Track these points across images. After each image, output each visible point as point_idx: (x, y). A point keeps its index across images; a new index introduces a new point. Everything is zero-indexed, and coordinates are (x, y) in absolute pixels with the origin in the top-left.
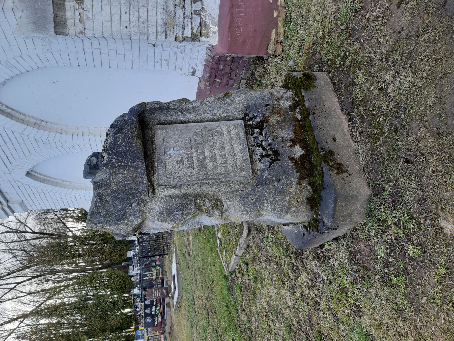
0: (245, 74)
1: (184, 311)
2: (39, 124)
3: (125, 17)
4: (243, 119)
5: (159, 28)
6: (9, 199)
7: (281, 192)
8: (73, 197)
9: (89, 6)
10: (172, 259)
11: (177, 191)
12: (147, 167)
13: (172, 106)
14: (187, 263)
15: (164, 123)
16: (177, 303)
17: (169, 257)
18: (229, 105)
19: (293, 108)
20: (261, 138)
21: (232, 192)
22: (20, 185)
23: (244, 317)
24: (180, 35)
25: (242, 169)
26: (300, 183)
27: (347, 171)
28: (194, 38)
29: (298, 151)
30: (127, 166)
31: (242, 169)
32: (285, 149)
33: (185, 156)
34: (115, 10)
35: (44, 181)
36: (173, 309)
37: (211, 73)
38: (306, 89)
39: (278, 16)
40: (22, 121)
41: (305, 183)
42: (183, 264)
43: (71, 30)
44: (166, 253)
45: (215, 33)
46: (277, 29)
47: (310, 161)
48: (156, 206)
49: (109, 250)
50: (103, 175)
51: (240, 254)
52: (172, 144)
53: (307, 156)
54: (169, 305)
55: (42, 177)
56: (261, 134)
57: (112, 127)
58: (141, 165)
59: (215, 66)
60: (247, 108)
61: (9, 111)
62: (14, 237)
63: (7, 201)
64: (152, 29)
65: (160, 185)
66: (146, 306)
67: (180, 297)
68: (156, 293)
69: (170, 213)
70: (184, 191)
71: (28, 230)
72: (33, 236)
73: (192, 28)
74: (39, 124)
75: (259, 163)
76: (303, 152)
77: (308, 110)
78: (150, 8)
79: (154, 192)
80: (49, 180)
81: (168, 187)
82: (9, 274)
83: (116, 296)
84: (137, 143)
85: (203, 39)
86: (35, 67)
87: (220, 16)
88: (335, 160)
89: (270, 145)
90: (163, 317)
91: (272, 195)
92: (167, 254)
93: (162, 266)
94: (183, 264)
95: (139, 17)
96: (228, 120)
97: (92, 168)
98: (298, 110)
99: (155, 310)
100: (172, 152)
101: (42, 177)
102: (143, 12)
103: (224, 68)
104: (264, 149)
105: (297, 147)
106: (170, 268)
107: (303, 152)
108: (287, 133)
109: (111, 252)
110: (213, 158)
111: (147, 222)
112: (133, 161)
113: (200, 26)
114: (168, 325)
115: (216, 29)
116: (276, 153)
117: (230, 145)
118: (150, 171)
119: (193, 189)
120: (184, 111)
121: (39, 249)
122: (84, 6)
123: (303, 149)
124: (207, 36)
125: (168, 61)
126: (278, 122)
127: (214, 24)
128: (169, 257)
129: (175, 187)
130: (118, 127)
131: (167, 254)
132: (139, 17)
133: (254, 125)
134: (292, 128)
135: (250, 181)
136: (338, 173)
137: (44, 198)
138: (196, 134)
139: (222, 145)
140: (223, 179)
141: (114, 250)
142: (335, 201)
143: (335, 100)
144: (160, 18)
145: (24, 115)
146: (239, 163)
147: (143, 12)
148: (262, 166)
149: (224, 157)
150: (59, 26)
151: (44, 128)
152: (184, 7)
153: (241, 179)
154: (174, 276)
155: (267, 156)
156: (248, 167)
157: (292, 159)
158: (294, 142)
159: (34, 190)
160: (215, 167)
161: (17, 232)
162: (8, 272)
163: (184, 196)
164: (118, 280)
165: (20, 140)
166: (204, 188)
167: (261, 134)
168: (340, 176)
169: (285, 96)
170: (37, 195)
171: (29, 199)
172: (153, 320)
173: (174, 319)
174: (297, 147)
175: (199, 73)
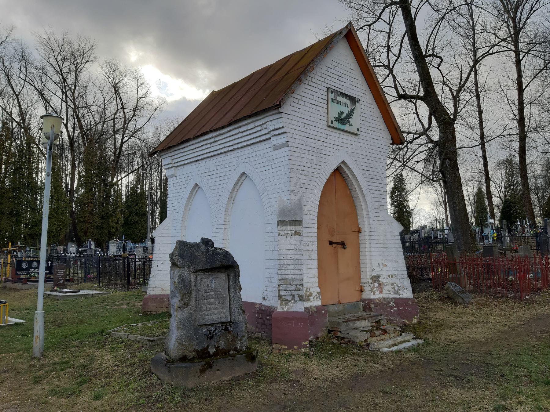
0: (265, 336)
2: (231, 199)
3: (289, 257)
4: (230, 322)
5: (284, 276)
6: (178, 168)
7: (190, 340)
8: (177, 211)
9: (293, 238)
10: (94, 290)
11: (193, 284)
12: (206, 269)
13: (237, 282)
14: (96, 304)
15: (228, 278)
16: (49, 295)
17: (96, 287)
18: (238, 313)
19: (236, 349)
20: (220, 330)
21: (191, 313)
22: (189, 178)
23: (75, 343)
24: (281, 288)
25: (203, 319)
26: (195, 351)
27: (201, 375)
28: (280, 297)
29: (212, 350)
30: (207, 259)
31: (203, 319)
32: (213, 343)
33: (211, 288)
34: (292, 252)
35: (191, 193)
37: (264, 311)
38: (246, 357)
39: (295, 349)
40: (233, 190)
41: (194, 353)
42: (94, 300)
43: (280, 228)
44: (101, 284)
45: (283, 309)
46: (287, 349)
47: (207, 357)
49: (94, 221)
50: (203, 248)
51: (129, 338)
52: (217, 282)
53: (210, 356)
55: (194, 193)
56: (222, 330)
57: (227, 252)
58: (207, 266)
59: (268, 313)
60: (237, 323)
61: (240, 183)
62: (119, 126)
63: (176, 167)
64: (283, 272)
65: (197, 275)
67: (57, 298)
69: (182, 280)
70: (193, 287)
71: (125, 139)
72: (119, 143)
73: (285, 295)
74: (231, 199)
75: (206, 329)
76: (211, 353)
77: (234, 356)
78: (294, 271)
79: (194, 272)
80: (191, 196)
81: (196, 280)
82: (77, 117)
84: (218, 264)
85: (279, 302)
86: (264, 204)
87: (293, 312)
88: (206, 369)
89: (216, 334)
91: (189, 335)
92: (99, 284)
93: (86, 280)
94: (94, 300)
95: (289, 265)
96: (230, 313)
97: (207, 242)
98: (235, 352)
100: (213, 282)
101: (194, 193)
102: (292, 267)
103: (268, 320)
104: (214, 331)
105: (214, 350)
106: (84, 288)
107: (211, 353)
108: (222, 345)
109: (91, 223)
110: (210, 303)
111: (178, 269)
112: (209, 262)
113: (286, 300)
114: (19, 286)
115: (286, 310)
116: (211, 338)
117: (217, 313)
118: (204, 271)
119: (194, 292)
120: (235, 288)
121: (102, 149)
122: (293, 236)
123: (213, 353)
124: (281, 304)
125: (270, 282)
126: (228, 339)
127: (288, 308)
128: (96, 287)
129: (195, 283)
130: (227, 255)
131: (99, 284)
132: (289, 265)
133: (227, 326)
134: (225, 347)
135: (197, 324)
136: (200, 369)
137: (177, 191)
138: (222, 295)
139: (216, 309)
140: (198, 308)
141: (94, 226)
142: (186, 367)
143: (240, 374)
144: (289, 277)
145: (237, 191)
146: (206, 317)
147: (292, 267)
148: (204, 331)
149: (210, 309)
150: (281, 223)
151: (229, 202)
152: (296, 290)
153: (198, 319)
154: (79, 291)
155: (210, 333)
156: (204, 322)
157: (208, 347)
158: (217, 348)
159: (185, 186)
160: (205, 304)
161: (124, 129)
162: (80, 116)
163: (190, 288)
164: (56, 230)
165: (221, 186)
166: (194, 298)
167: (222, 330)
168: (199, 371)
169: (243, 345)
170: (180, 187)
171: (177, 181)
172: (24, 270)
173: (28, 292)
174: (214, 350)
175: (264, 303)
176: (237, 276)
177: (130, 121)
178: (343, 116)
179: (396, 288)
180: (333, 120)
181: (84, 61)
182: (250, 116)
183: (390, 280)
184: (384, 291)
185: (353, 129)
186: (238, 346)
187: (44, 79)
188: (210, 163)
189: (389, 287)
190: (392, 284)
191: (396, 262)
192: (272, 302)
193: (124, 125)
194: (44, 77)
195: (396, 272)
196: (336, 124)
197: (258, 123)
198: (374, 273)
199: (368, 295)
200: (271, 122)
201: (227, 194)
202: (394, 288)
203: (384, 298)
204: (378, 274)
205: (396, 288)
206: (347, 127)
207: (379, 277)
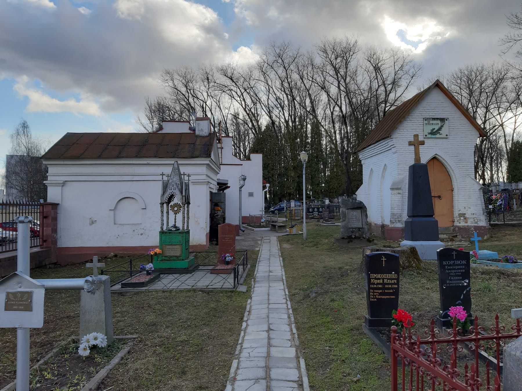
1: (316, 227)
19: (363, 237)
29: (353, 237)
32: (354, 234)
36: (317, 223)
48: (344, 210)
52: (357, 213)
54: (319, 221)
66: (318, 209)
68: (326, 214)
83: (323, 185)
90: (312, 218)
99: (316, 214)
108: (357, 235)
176: (366, 211)
177: (390, 93)
178: (434, 131)
179: (476, 221)
180: (427, 134)
181: (351, 53)
182: (383, 139)
183: (472, 216)
184: (469, 222)
185: (444, 136)
186: (364, 236)
187: (325, 74)
188: (374, 159)
189: (472, 220)
190: (474, 218)
191: (476, 206)
192: (387, 222)
193: (386, 97)
194: (325, 73)
195: (476, 212)
196: (430, 136)
197: (386, 142)
198: (460, 212)
199: (456, 224)
200: (388, 143)
201: (381, 174)
202: (475, 220)
203: (468, 226)
204: (464, 212)
205: (476, 221)
206: (438, 136)
207: (465, 214)
